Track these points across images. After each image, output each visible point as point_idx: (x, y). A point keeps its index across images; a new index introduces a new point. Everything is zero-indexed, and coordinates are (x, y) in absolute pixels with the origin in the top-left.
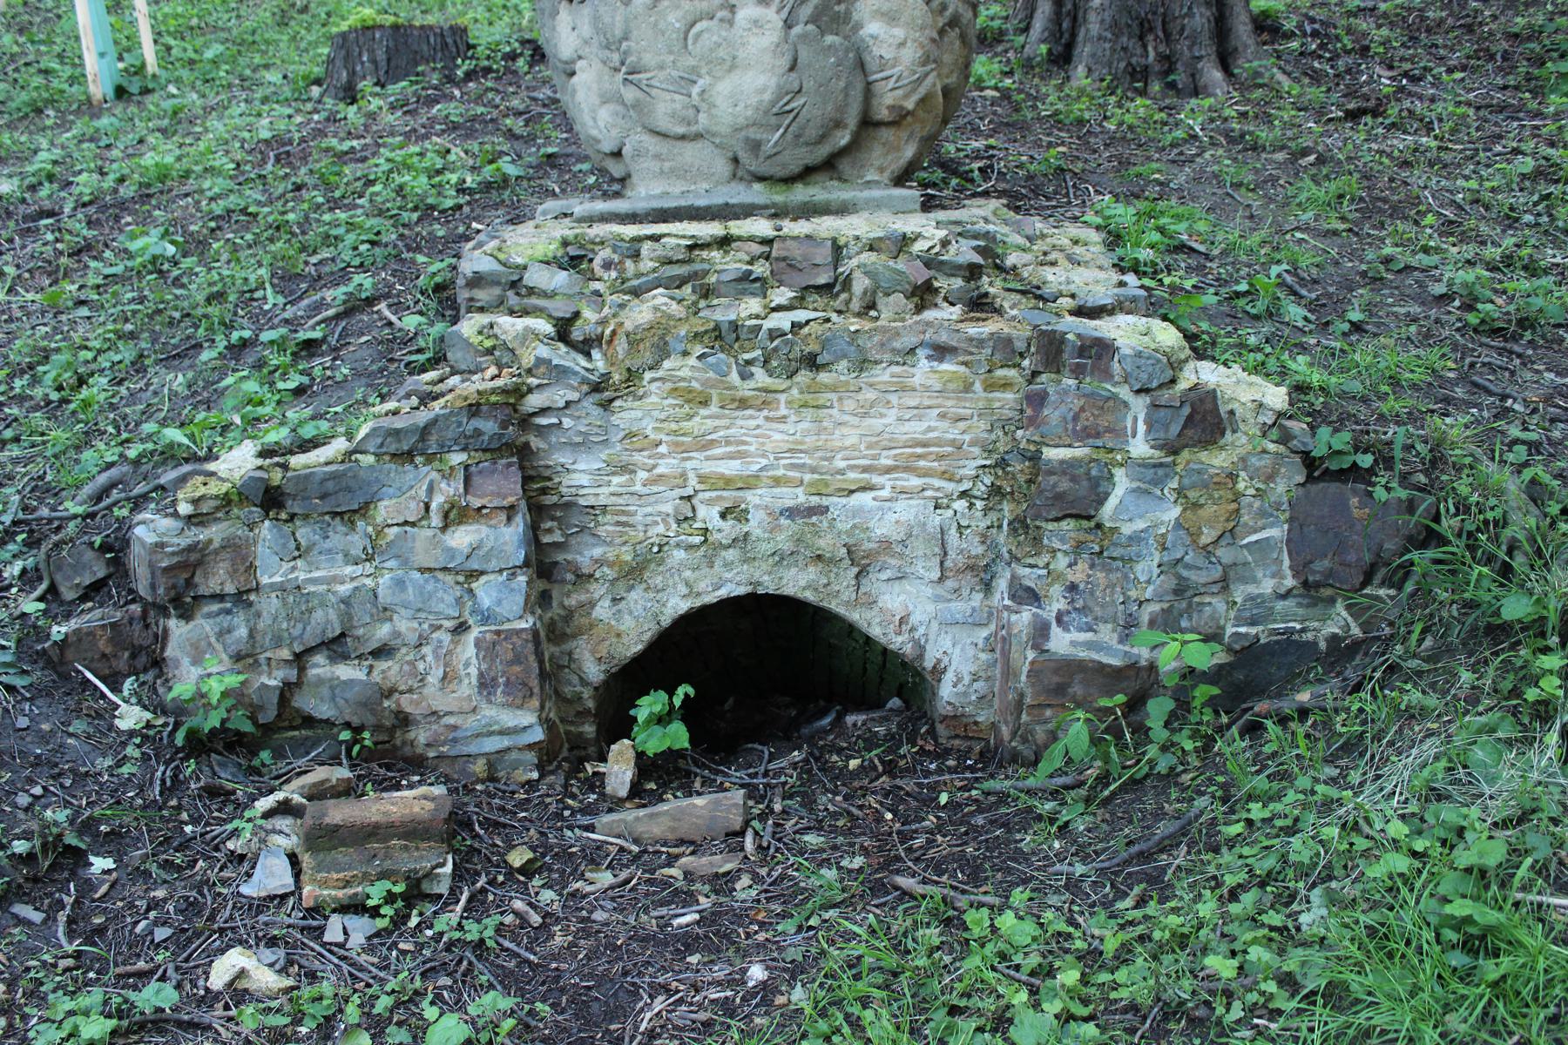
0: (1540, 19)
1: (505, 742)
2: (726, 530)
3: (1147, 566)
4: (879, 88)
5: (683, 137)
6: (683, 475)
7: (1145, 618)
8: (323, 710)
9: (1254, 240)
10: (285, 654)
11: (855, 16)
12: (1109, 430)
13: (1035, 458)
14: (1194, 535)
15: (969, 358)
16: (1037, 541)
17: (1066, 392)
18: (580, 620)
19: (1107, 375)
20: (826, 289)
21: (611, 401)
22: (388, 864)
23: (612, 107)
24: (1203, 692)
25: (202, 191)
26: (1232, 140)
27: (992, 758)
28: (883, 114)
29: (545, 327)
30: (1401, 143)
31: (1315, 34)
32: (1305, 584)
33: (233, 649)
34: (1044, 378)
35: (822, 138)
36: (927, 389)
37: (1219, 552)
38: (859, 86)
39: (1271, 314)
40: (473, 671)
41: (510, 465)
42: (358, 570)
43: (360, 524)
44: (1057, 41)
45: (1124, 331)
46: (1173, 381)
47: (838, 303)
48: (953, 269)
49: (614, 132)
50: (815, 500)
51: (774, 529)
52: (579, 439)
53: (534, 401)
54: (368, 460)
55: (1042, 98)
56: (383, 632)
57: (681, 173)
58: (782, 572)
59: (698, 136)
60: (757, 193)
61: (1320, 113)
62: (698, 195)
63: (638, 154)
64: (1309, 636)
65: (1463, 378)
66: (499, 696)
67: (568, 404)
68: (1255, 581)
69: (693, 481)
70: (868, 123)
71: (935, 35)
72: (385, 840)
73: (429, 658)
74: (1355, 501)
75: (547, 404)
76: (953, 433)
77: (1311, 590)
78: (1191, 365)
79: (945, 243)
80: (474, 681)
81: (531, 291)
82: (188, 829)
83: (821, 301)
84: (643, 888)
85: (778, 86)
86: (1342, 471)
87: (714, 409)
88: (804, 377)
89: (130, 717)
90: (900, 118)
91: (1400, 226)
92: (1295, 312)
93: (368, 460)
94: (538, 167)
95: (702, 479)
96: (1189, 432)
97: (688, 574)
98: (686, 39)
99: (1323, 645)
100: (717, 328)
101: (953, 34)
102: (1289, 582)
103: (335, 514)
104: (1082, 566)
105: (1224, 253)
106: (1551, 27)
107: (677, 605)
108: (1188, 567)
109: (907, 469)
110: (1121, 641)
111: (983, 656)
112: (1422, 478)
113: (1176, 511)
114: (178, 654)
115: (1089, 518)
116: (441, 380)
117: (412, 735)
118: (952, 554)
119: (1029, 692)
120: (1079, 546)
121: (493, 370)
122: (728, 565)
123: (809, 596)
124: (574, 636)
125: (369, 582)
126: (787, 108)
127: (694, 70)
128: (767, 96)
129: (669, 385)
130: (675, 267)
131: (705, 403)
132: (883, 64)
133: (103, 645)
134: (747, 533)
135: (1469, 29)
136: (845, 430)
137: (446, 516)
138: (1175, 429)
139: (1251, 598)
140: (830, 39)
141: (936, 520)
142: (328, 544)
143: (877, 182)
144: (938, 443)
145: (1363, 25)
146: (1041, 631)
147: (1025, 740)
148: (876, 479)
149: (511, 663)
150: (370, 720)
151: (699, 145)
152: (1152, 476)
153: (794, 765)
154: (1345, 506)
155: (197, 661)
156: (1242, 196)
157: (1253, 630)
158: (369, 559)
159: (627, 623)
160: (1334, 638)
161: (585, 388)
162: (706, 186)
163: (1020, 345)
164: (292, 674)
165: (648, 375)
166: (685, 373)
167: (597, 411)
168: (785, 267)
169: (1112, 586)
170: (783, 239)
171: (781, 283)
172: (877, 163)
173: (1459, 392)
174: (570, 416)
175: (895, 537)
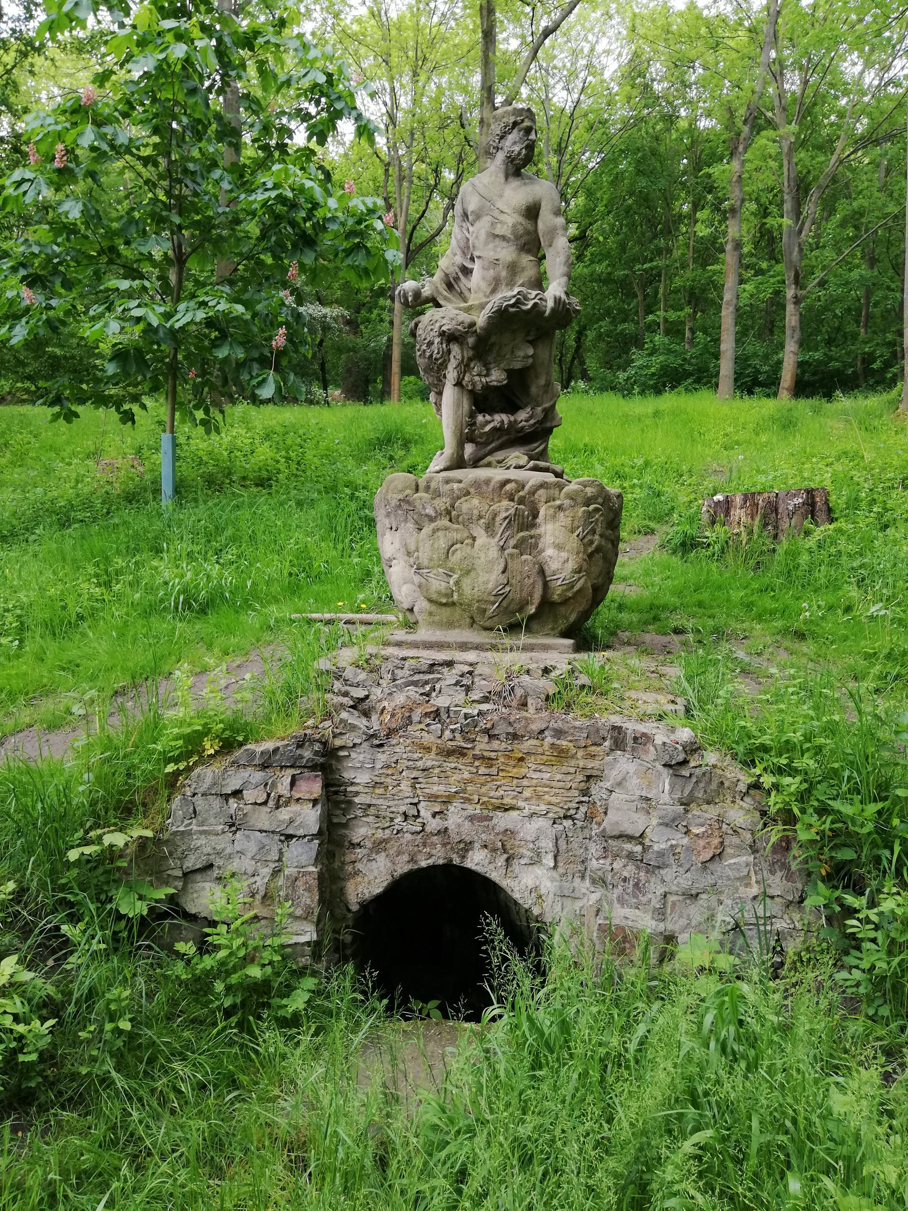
4: (552, 585)
5: (445, 605)
41: (317, 776)
49: (410, 599)
52: (359, 765)
134: (446, 829)
161: (364, 737)
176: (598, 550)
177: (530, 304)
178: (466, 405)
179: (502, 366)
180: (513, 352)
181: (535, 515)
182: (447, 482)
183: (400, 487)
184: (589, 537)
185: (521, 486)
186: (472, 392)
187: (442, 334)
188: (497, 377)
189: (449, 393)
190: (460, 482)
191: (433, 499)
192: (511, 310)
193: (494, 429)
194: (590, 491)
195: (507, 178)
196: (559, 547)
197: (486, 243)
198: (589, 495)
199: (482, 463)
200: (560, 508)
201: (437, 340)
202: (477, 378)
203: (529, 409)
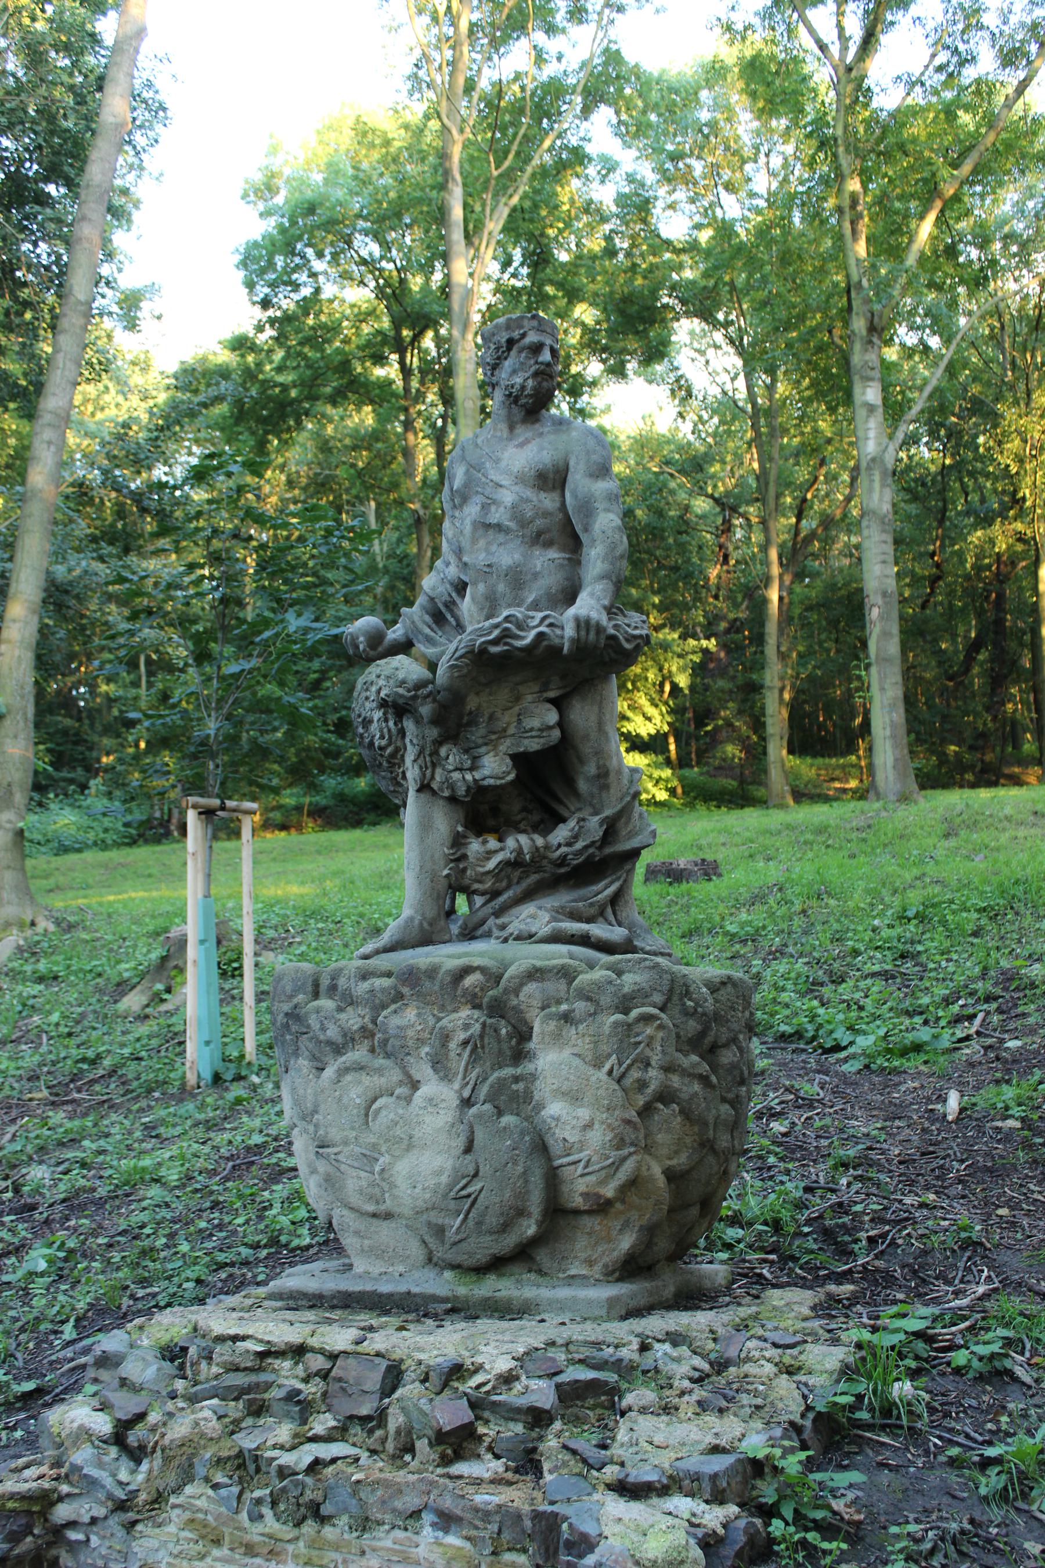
4: (567, 1172)
11: (537, 1096)
15: (474, 1533)
21: (134, 1523)
35: (505, 1227)
53: (62, 1512)
59: (388, 1216)
67: (94, 1521)
71: (632, 1115)
75: (73, 1517)
85: (454, 1168)
88: (309, 1527)
98: (367, 1115)
100: (240, 1454)
126: (464, 1193)
128: (444, 1179)
129: (188, 1515)
130: (241, 1374)
143: (584, 1277)
162: (401, 1269)
165: (173, 1500)
167: (120, 1533)
172: (583, 1255)
174: (97, 1534)
176: (665, 1096)
177: (530, 637)
179: (502, 748)
180: (519, 721)
181: (523, 1034)
183: (289, 992)
184: (635, 1074)
185: (494, 977)
186: (453, 800)
187: (383, 704)
190: (389, 974)
191: (340, 1009)
192: (494, 649)
193: (507, 863)
195: (511, 428)
196: (574, 1097)
197: (474, 541)
198: (626, 990)
199: (480, 932)
200: (567, 1018)
201: (377, 715)
202: (456, 775)
203: (572, 823)
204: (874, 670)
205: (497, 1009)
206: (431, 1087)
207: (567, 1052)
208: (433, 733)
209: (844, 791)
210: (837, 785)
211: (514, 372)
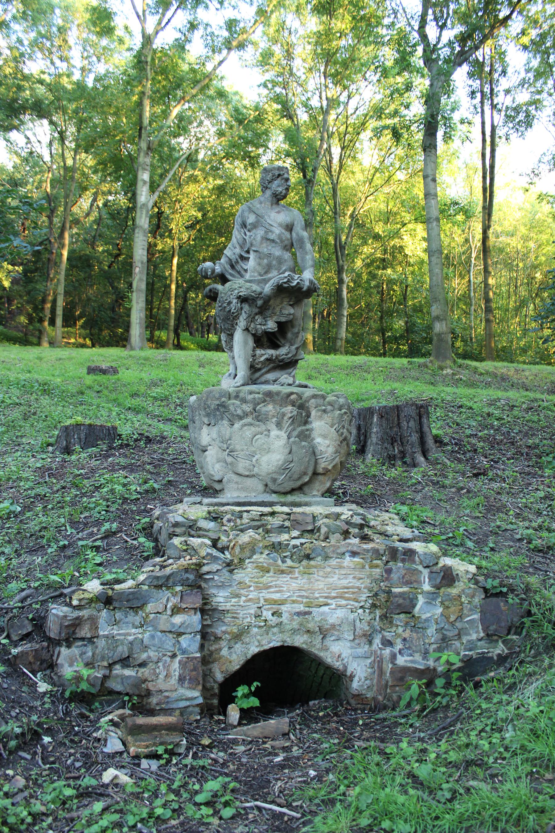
0: (537, 441)
1: (188, 703)
2: (274, 620)
3: (431, 631)
4: (320, 461)
5: (247, 476)
6: (259, 599)
7: (431, 650)
8: (118, 688)
9: (450, 519)
10: (105, 664)
12: (415, 581)
13: (389, 592)
14: (447, 618)
16: (391, 622)
17: (399, 568)
18: (215, 656)
19: (414, 562)
20: (311, 531)
22: (162, 740)
23: (221, 464)
24: (455, 675)
25: (20, 487)
26: (434, 484)
27: (377, 708)
28: (320, 470)
29: (209, 542)
30: (496, 486)
31: (456, 444)
32: (488, 635)
33: (86, 660)
34: (391, 563)
35: (299, 478)
36: (349, 567)
37: (457, 624)
38: (313, 460)
39: (462, 545)
40: (177, 674)
42: (137, 631)
43: (140, 612)
44: (359, 444)
45: (417, 546)
46: (437, 563)
47: (316, 536)
48: (355, 525)
49: (221, 473)
50: (307, 609)
51: (292, 620)
53: (205, 569)
54: (145, 587)
55: (358, 467)
56: (144, 656)
57: (244, 489)
58: (294, 637)
59: (253, 476)
60: (274, 498)
61: (463, 474)
62: (251, 497)
63: (229, 481)
64: (490, 655)
65: (531, 566)
66: (186, 684)
68: (470, 634)
69: (262, 601)
70: (315, 473)
72: (159, 731)
73: (161, 668)
74: (502, 604)
76: (358, 584)
77: (490, 637)
78: (442, 558)
79: (352, 516)
80: (177, 678)
81: (200, 529)
82: (76, 728)
83: (309, 536)
84: (257, 752)
86: (497, 593)
87: (271, 574)
88: (305, 562)
89: (43, 687)
90: (326, 472)
91: (501, 515)
92: (470, 544)
93: (145, 587)
94: (165, 485)
95: (266, 600)
96: (444, 582)
97: (259, 637)
99: (495, 658)
100: (273, 544)
101: (345, 443)
102: (482, 634)
103: (131, 608)
104: (408, 631)
105: (440, 524)
106: (541, 444)
107: (254, 650)
108: (446, 630)
109: (341, 597)
110: (423, 659)
111: (369, 670)
112: (524, 596)
113: (440, 610)
114: (63, 662)
115: (410, 613)
116: (165, 561)
117: (150, 700)
118: (358, 630)
119: (390, 680)
120: (407, 624)
121: (188, 557)
122: (274, 634)
123: (304, 646)
124: (213, 662)
125: (140, 636)
127: (254, 452)
128: (280, 463)
131: (268, 572)
132: (322, 453)
133: (31, 659)
135: (512, 443)
136: (319, 583)
137: (172, 611)
138: (438, 580)
139: (469, 641)
140: (303, 443)
141: (352, 616)
142: (127, 620)
144: (352, 587)
145: (473, 441)
146: (393, 657)
147: (389, 700)
148: (330, 601)
149: (192, 671)
150: (137, 692)
151: (253, 479)
152: (432, 597)
153: (298, 715)
154: (499, 606)
155: (71, 665)
156: (442, 503)
157: (470, 653)
158: (142, 626)
159: (234, 657)
160: (499, 655)
163: (382, 552)
164: (107, 672)
165: (247, 561)
166: (261, 560)
167: (227, 574)
168: (296, 524)
169: (419, 638)
170: (295, 513)
171: (294, 529)
173: (531, 570)
175: (337, 623)
177: (295, 283)
178: (251, 343)
181: (308, 416)
182: (251, 393)
186: (254, 335)
187: (239, 297)
188: (271, 326)
189: (238, 336)
192: (286, 285)
193: (267, 359)
194: (342, 401)
196: (325, 437)
197: (261, 243)
200: (324, 411)
202: (259, 326)
204: (134, 294)
205: (301, 407)
206: (275, 432)
207: (323, 423)
208: (257, 310)
209: (69, 343)
210: (65, 340)
211: (279, 186)
